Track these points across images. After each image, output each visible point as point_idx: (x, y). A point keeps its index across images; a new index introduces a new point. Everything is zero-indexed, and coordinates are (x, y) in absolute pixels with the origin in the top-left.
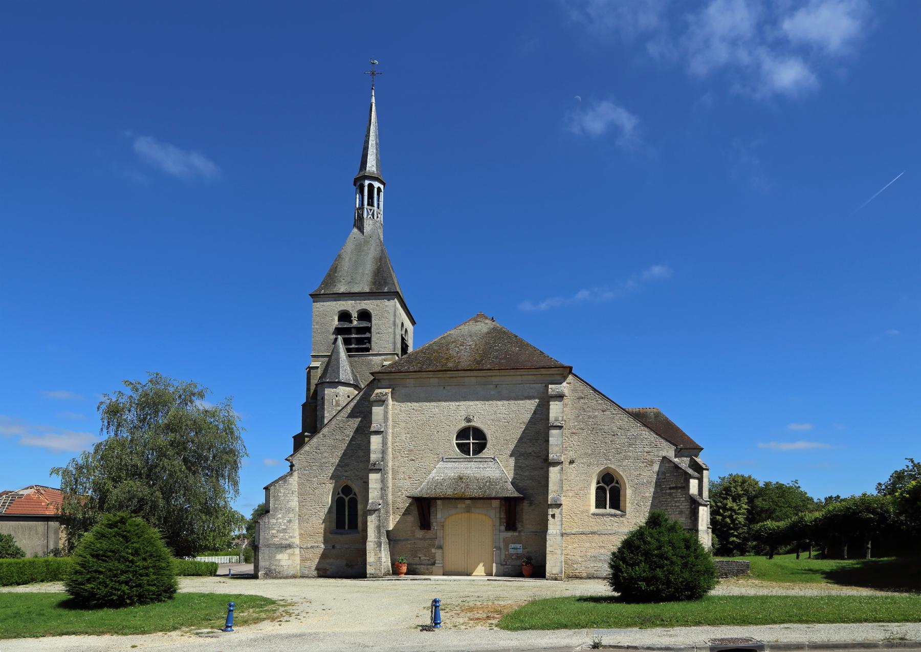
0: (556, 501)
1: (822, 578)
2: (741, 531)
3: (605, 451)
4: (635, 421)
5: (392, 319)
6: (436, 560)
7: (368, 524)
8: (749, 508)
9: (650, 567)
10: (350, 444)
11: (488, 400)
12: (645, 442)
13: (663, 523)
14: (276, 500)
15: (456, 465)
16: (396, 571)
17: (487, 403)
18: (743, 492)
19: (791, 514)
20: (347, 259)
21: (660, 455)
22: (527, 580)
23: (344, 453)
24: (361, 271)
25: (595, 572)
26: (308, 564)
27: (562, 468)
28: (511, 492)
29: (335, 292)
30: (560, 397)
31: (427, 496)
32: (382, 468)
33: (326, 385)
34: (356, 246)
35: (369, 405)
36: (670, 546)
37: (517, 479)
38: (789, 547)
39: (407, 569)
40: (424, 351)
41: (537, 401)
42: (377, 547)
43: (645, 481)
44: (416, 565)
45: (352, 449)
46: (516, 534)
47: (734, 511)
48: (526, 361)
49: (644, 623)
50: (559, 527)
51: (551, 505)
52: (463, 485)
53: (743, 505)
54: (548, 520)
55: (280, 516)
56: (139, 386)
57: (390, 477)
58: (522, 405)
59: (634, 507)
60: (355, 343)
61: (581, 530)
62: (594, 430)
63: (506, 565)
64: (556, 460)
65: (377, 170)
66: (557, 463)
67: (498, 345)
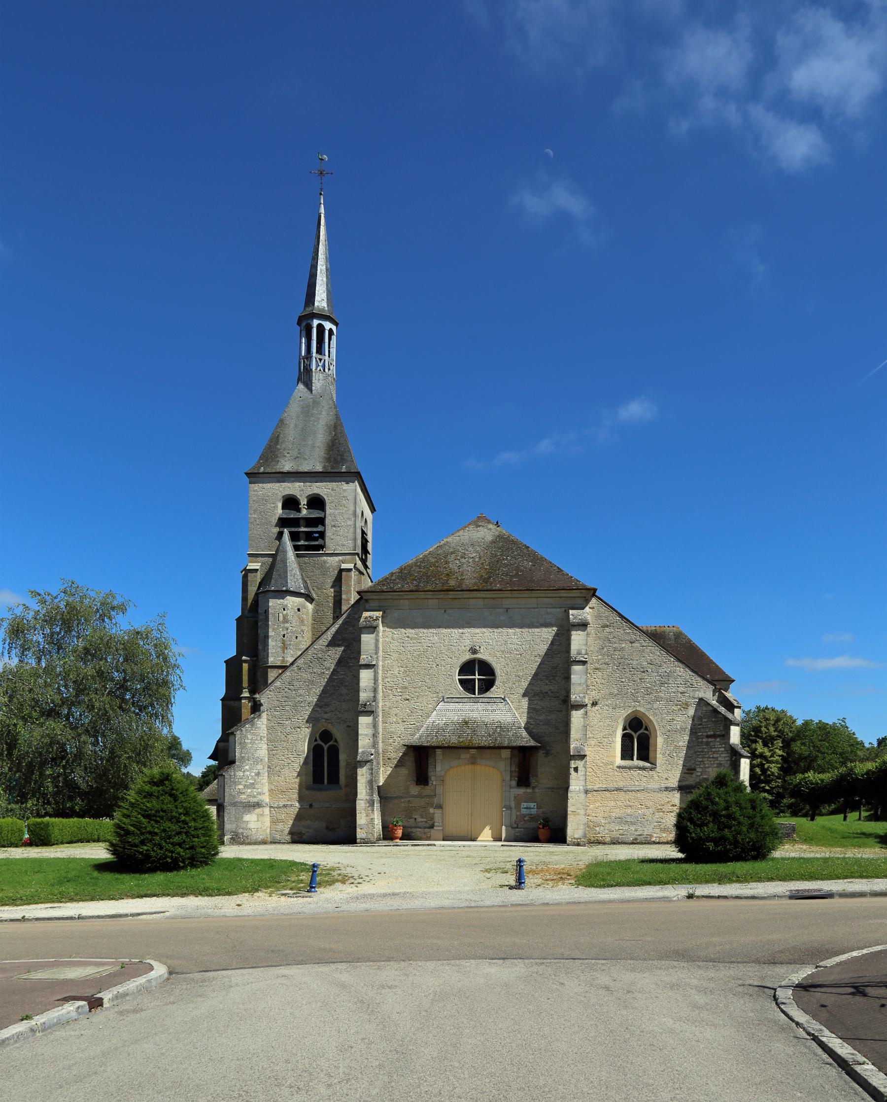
0: (580, 752)
1: (876, 842)
2: (773, 784)
3: (633, 691)
4: (668, 654)
5: (352, 508)
6: (434, 822)
7: (358, 778)
8: (785, 754)
9: (718, 827)
10: (330, 679)
11: (497, 627)
12: (680, 681)
13: (729, 783)
14: (242, 748)
15: (459, 706)
16: (388, 835)
17: (495, 630)
18: (776, 733)
19: (836, 762)
20: (292, 426)
21: (696, 696)
22: (545, 845)
23: (323, 689)
24: (310, 443)
25: (620, 837)
26: (280, 826)
27: (586, 712)
28: (525, 740)
29: (278, 471)
30: (583, 625)
31: (428, 744)
32: (374, 709)
33: (271, 594)
34: (303, 408)
35: (354, 631)
36: (737, 806)
37: (531, 724)
38: (833, 806)
39: (402, 833)
40: (419, 564)
41: (555, 629)
42: (369, 807)
43: (678, 727)
44: (411, 828)
45: (333, 686)
46: (529, 790)
47: (765, 758)
48: (542, 580)
49: (721, 879)
50: (582, 783)
51: (574, 756)
52: (469, 731)
53: (777, 751)
54: (570, 774)
55: (247, 767)
56: (48, 598)
57: (381, 720)
58: (538, 634)
59: (666, 758)
60: (305, 538)
61: (604, 786)
62: (621, 665)
63: (517, 828)
64: (579, 702)
65: (328, 305)
66: (580, 706)
67: (507, 558)
